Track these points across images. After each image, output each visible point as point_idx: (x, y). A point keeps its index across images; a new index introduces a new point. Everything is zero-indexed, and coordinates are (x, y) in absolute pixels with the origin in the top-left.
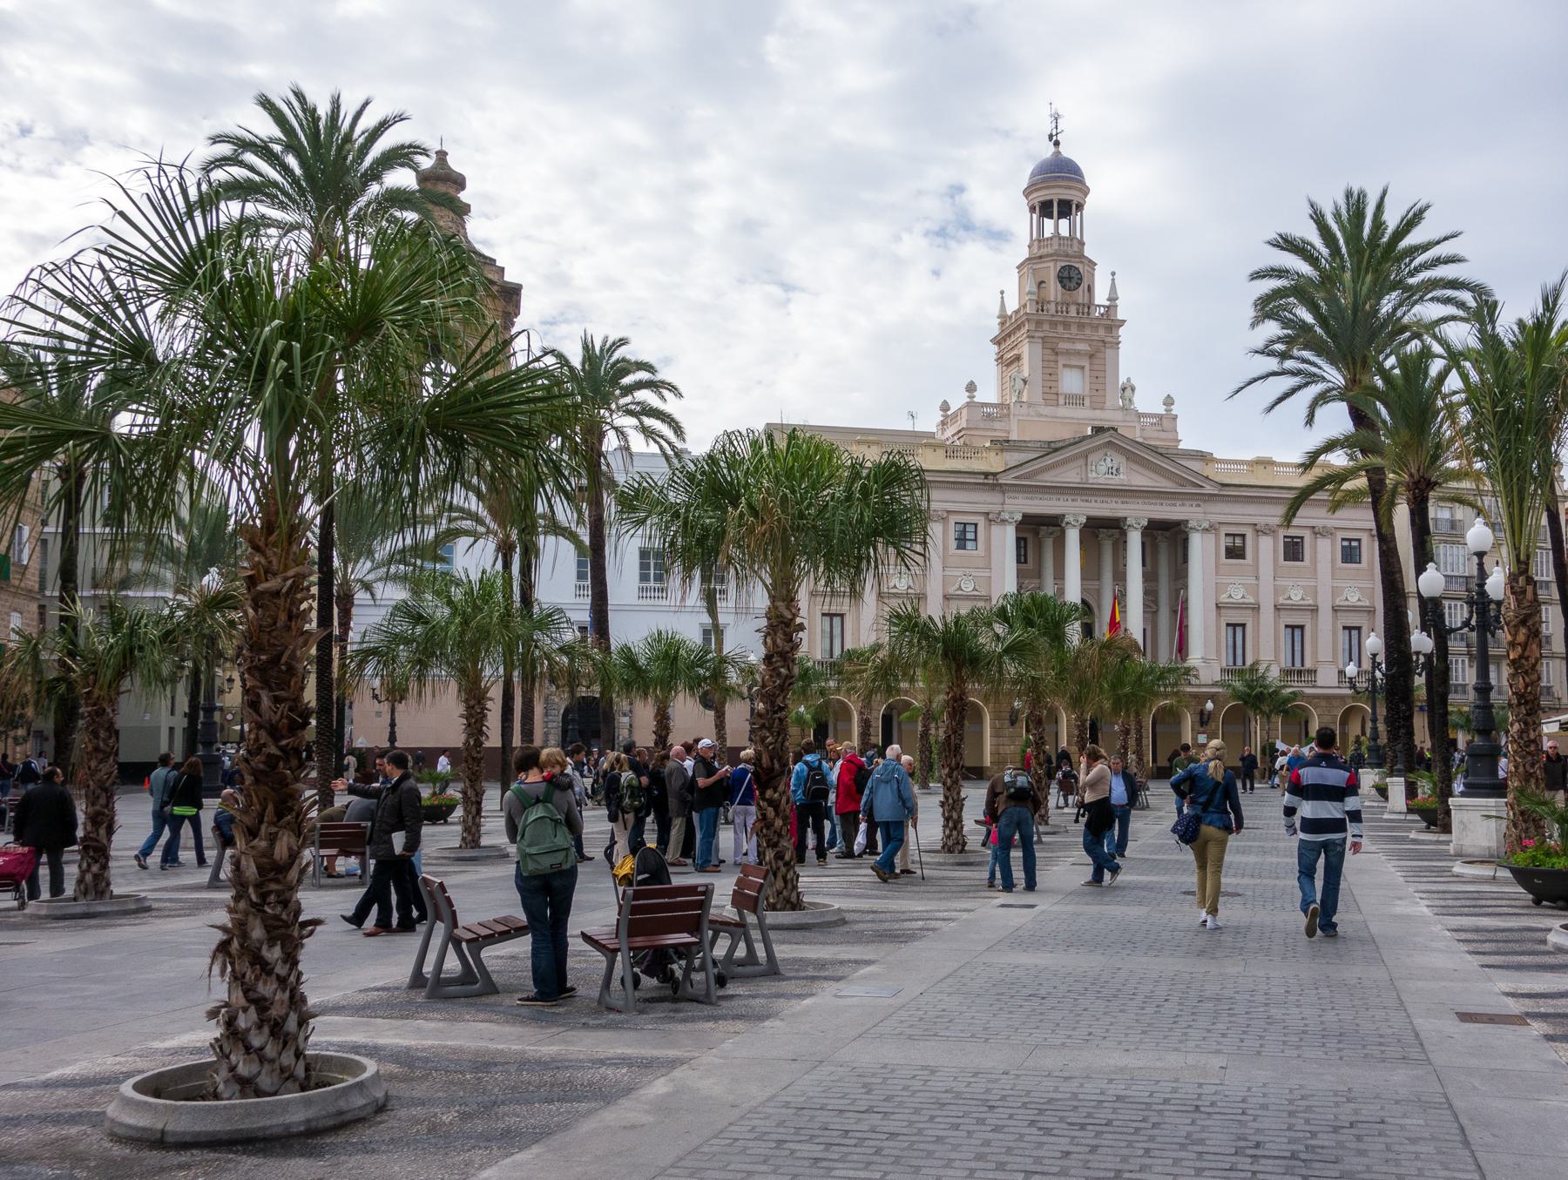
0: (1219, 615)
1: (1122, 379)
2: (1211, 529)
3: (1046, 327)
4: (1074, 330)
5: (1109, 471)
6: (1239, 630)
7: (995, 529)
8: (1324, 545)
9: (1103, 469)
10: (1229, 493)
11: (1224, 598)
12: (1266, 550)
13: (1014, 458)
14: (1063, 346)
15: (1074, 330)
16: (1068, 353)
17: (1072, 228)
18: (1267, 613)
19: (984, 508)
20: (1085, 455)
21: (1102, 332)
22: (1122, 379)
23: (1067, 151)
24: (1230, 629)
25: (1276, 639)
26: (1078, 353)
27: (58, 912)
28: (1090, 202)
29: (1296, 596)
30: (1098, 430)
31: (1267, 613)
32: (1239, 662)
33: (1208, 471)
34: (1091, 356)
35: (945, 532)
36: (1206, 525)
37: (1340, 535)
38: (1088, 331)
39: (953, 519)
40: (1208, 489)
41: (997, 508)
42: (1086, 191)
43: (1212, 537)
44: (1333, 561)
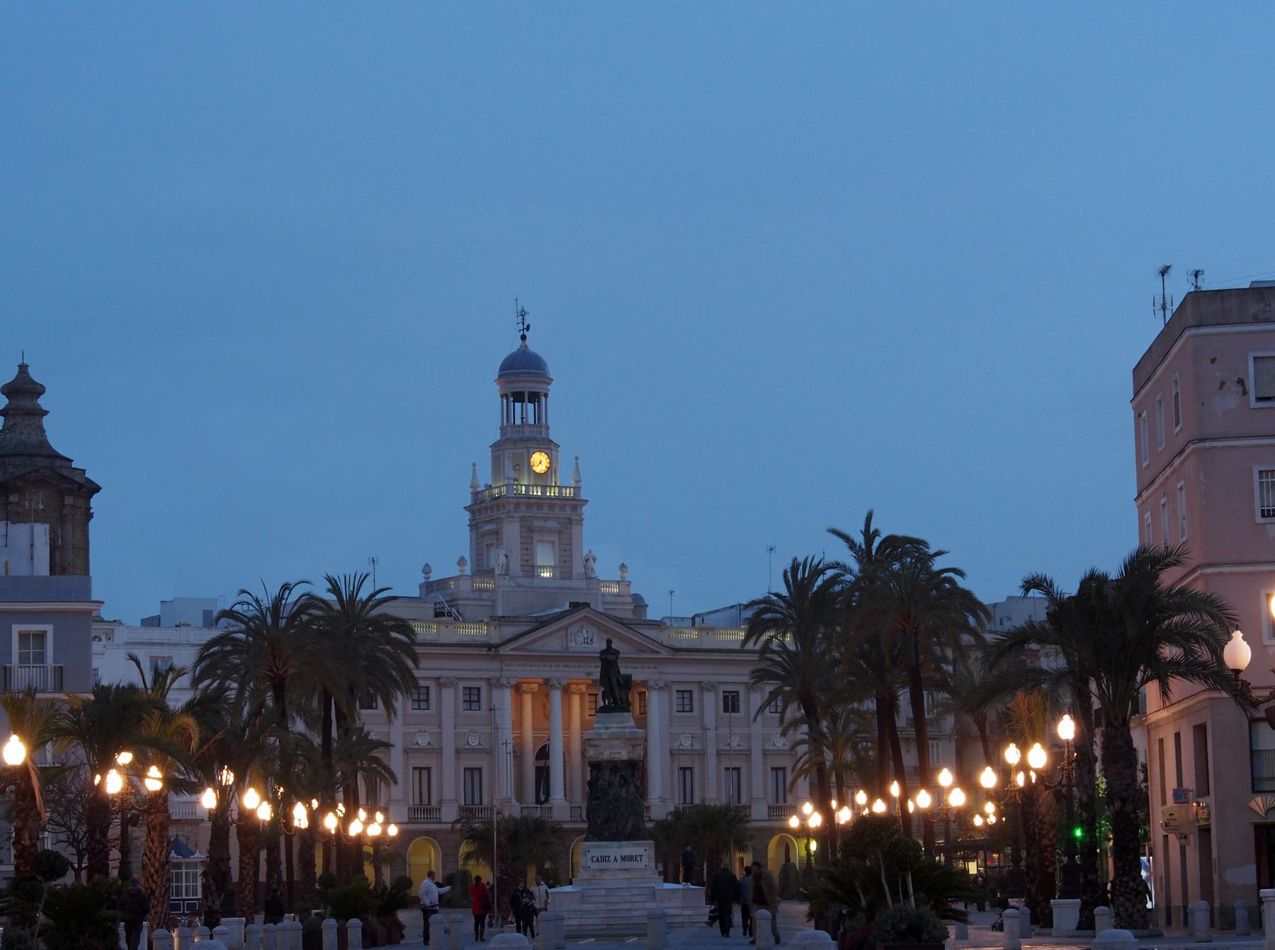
0: (672, 760)
1: (585, 552)
2: (666, 687)
3: (523, 508)
4: (545, 510)
5: (586, 641)
6: (425, 773)
7: (495, 693)
8: (709, 698)
9: (581, 639)
10: (681, 654)
11: (769, 747)
12: (710, 704)
13: (509, 631)
14: (536, 523)
15: (545, 510)
16: (541, 530)
17: (538, 417)
18: (712, 759)
19: (486, 675)
20: (566, 628)
21: (568, 511)
22: (585, 552)
23: (533, 346)
24: (417, 772)
25: (765, 780)
26: (550, 531)
27: (1173, 915)
28: (553, 390)
29: (423, 741)
30: (575, 606)
31: (712, 759)
32: (688, 800)
33: (662, 637)
34: (560, 533)
35: (456, 694)
36: (661, 684)
37: (722, 688)
38: (557, 511)
39: (462, 685)
40: (664, 654)
41: (497, 674)
42: (548, 381)
43: (665, 694)
44: (717, 712)
